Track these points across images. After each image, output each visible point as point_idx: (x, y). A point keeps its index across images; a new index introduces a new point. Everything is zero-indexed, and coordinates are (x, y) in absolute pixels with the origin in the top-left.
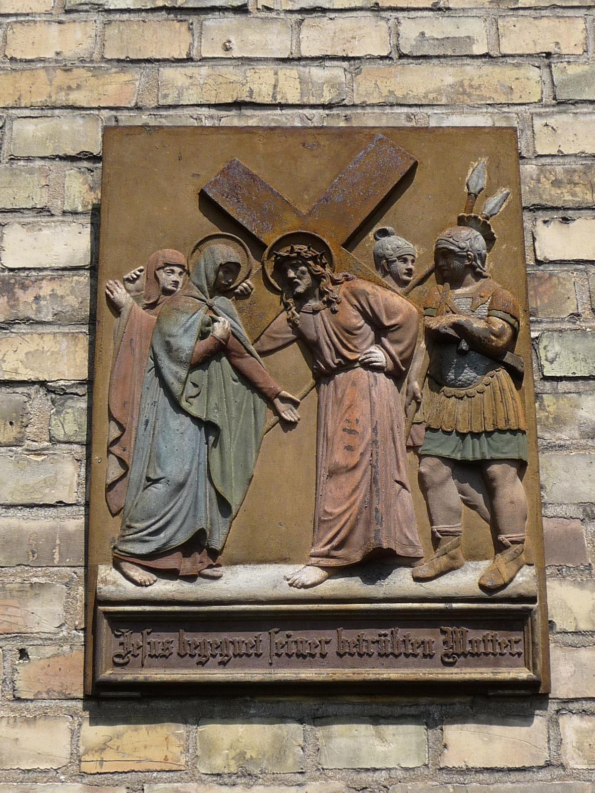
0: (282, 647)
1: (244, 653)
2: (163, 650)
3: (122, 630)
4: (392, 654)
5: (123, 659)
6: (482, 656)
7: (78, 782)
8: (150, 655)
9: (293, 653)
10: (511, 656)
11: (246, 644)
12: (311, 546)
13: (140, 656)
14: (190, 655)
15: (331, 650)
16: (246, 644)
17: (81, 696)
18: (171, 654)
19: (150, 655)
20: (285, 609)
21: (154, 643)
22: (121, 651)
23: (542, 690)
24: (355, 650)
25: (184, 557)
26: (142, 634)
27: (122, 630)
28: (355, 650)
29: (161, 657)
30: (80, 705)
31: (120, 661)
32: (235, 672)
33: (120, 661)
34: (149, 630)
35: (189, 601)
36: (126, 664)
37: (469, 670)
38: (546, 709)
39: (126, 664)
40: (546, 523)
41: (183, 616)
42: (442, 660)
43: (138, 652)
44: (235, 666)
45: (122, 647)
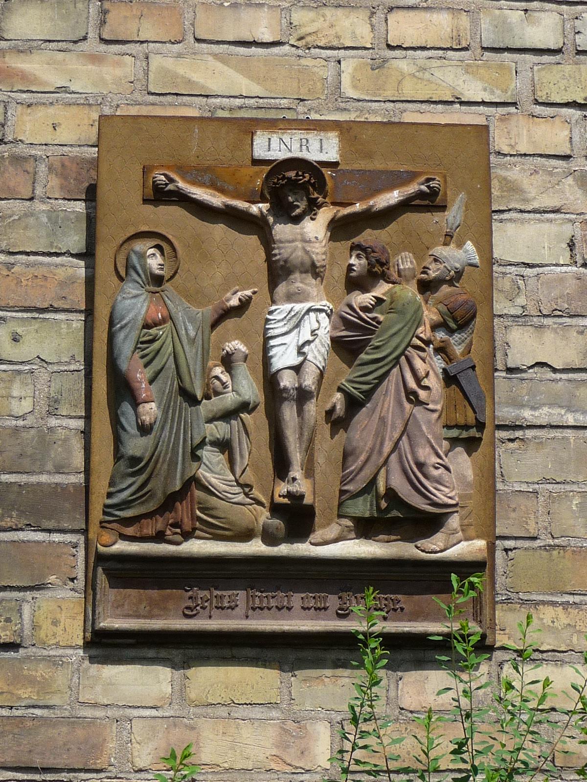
2: (229, 602)
5: (192, 611)
6: (266, 611)
8: (216, 607)
9: (273, 606)
11: (259, 597)
12: (249, 357)
13: (208, 608)
14: (287, 608)
17: (81, 642)
18: (237, 606)
19: (216, 607)
21: (379, 598)
22: (190, 603)
25: (326, 411)
30: (81, 652)
31: (187, 612)
33: (187, 612)
36: (195, 615)
38: (18, 652)
39: (195, 615)
40: (406, 352)
42: (183, 612)
43: (206, 604)
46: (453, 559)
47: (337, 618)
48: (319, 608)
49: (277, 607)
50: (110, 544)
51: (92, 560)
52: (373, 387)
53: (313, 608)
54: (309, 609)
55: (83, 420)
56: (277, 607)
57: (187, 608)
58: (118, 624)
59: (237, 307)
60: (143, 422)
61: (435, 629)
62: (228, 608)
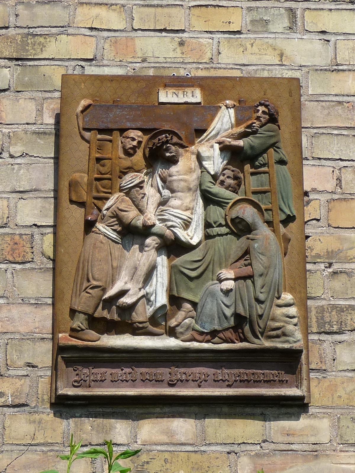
0: (190, 376)
1: (125, 380)
3: (77, 367)
4: (222, 380)
7: (57, 446)
9: (184, 380)
10: (111, 382)
15: (109, 378)
16: (273, 374)
20: (106, 353)
22: (76, 378)
23: (305, 401)
24: (276, 378)
26: (89, 369)
27: (77, 367)
28: (276, 378)
29: (100, 381)
31: (76, 384)
32: (187, 391)
33: (76, 384)
34: (93, 367)
35: (172, 350)
37: (114, 390)
41: (71, 359)
44: (179, 387)
45: (78, 376)
46: (161, 349)
47: (168, 387)
48: (256, 380)
49: (132, 380)
50: (95, 339)
51: (56, 348)
52: (161, 145)
53: (263, 381)
54: (218, 381)
55: (53, 198)
56: (132, 380)
57: (75, 381)
58: (71, 392)
59: (286, 219)
60: (84, 209)
61: (133, 393)
62: (100, 381)
